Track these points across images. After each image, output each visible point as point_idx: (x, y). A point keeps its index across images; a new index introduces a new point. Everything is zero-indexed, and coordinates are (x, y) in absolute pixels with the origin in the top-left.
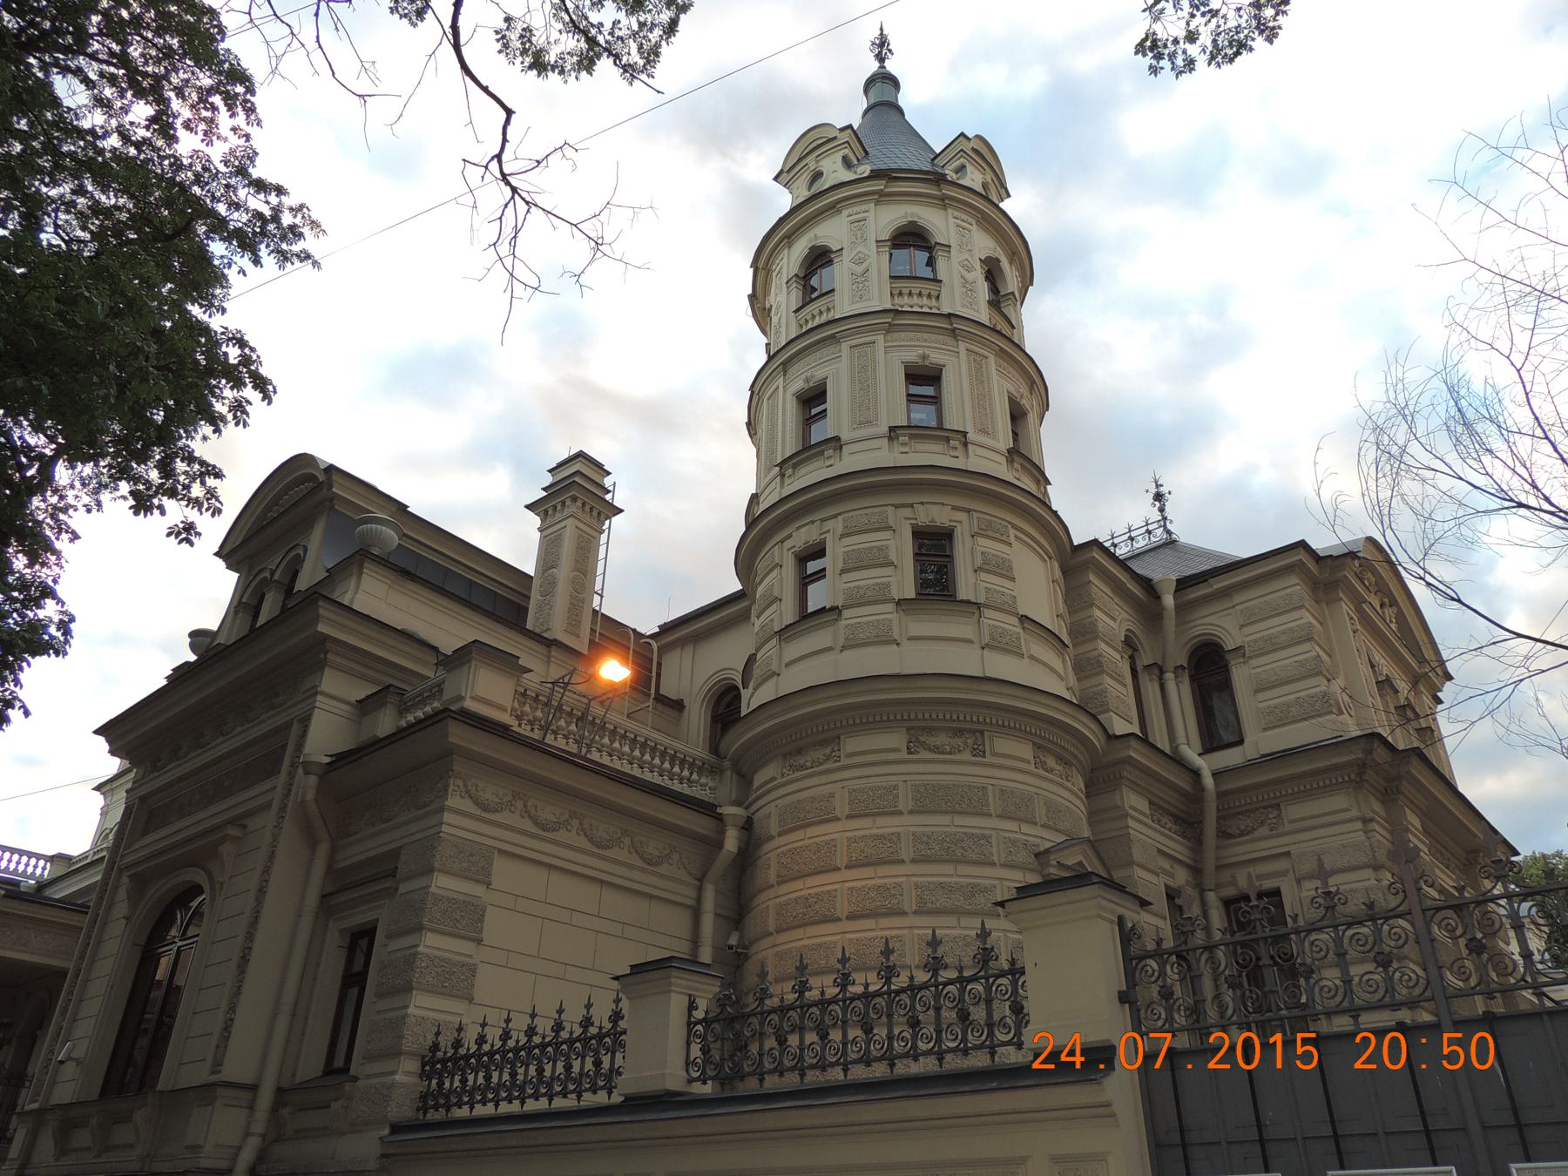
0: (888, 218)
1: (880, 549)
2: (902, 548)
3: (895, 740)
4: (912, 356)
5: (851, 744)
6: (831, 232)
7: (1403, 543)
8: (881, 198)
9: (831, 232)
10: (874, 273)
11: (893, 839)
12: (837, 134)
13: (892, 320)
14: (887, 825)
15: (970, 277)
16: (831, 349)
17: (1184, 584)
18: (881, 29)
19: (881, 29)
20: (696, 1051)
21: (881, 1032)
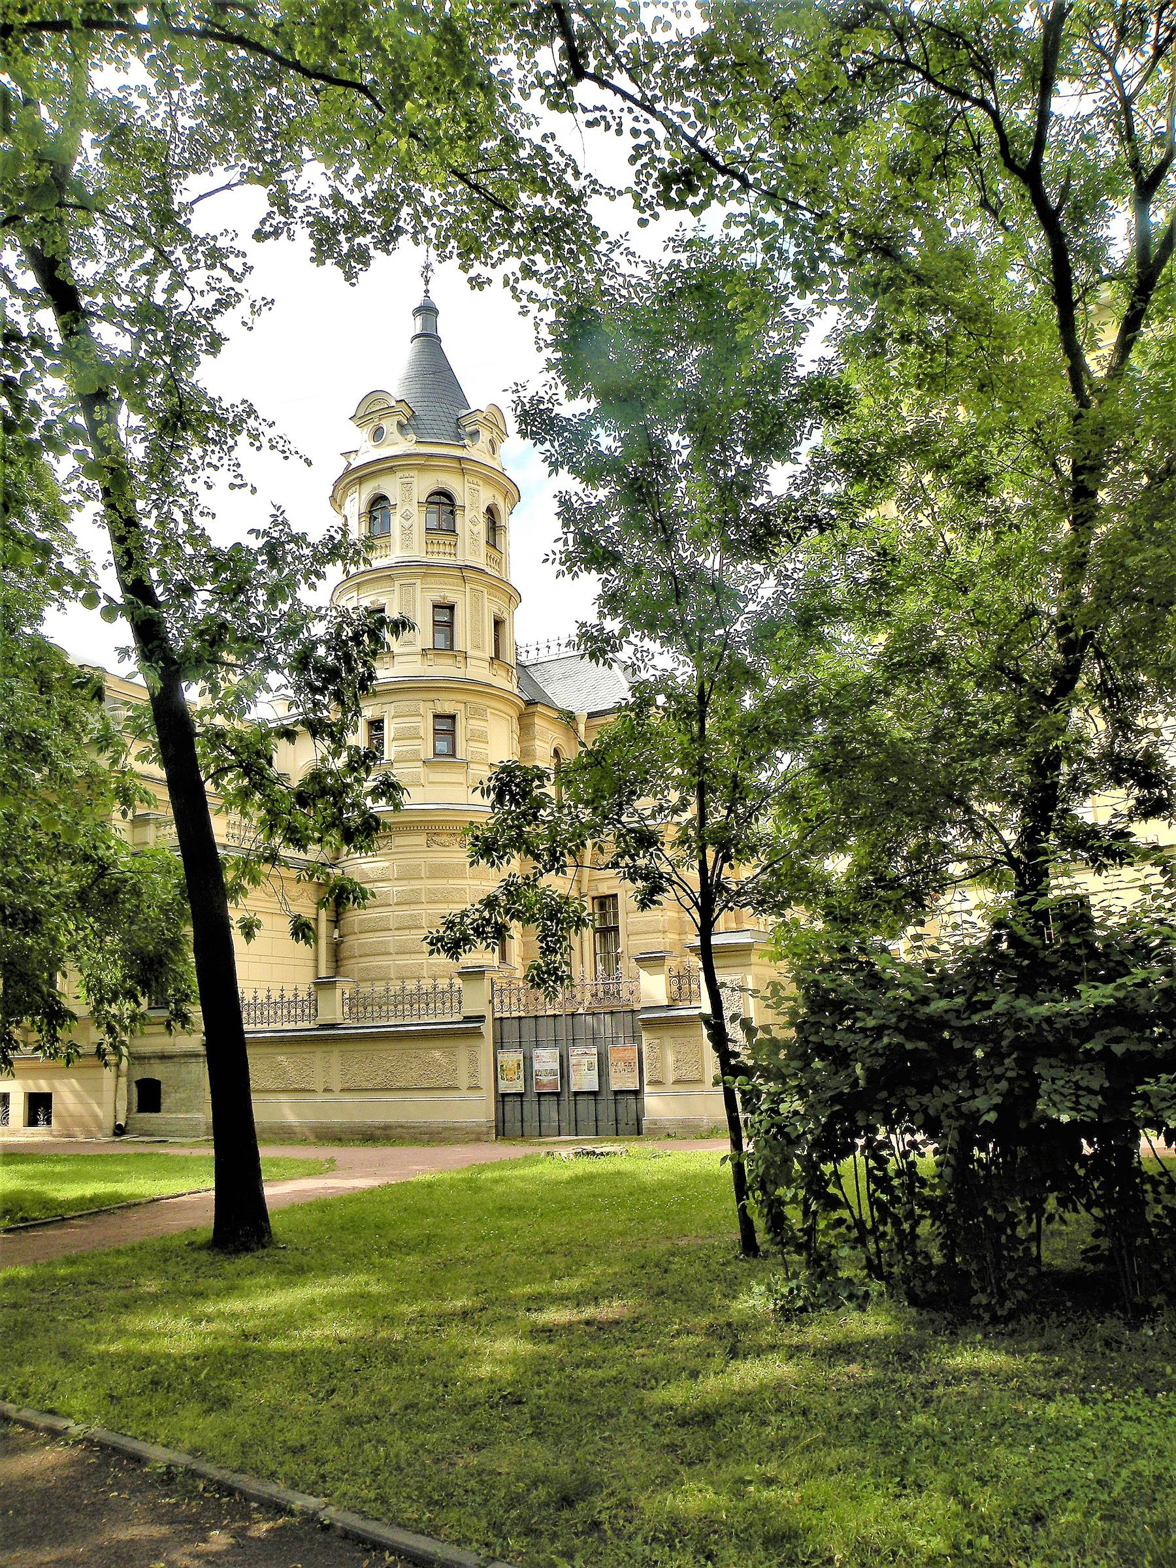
0: (425, 484)
1: (415, 728)
2: (426, 726)
3: (421, 839)
4: (436, 597)
5: (398, 841)
6: (390, 486)
7: (738, 1251)
8: (422, 468)
9: (390, 486)
10: (415, 529)
11: (417, 892)
12: (393, 403)
13: (426, 569)
14: (416, 885)
15: (475, 530)
16: (388, 583)
17: (591, 715)
18: (429, 340)
19: (429, 340)
20: (346, 1009)
21: (416, 1006)
